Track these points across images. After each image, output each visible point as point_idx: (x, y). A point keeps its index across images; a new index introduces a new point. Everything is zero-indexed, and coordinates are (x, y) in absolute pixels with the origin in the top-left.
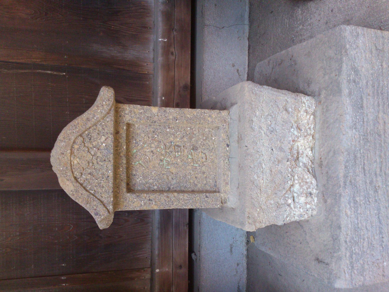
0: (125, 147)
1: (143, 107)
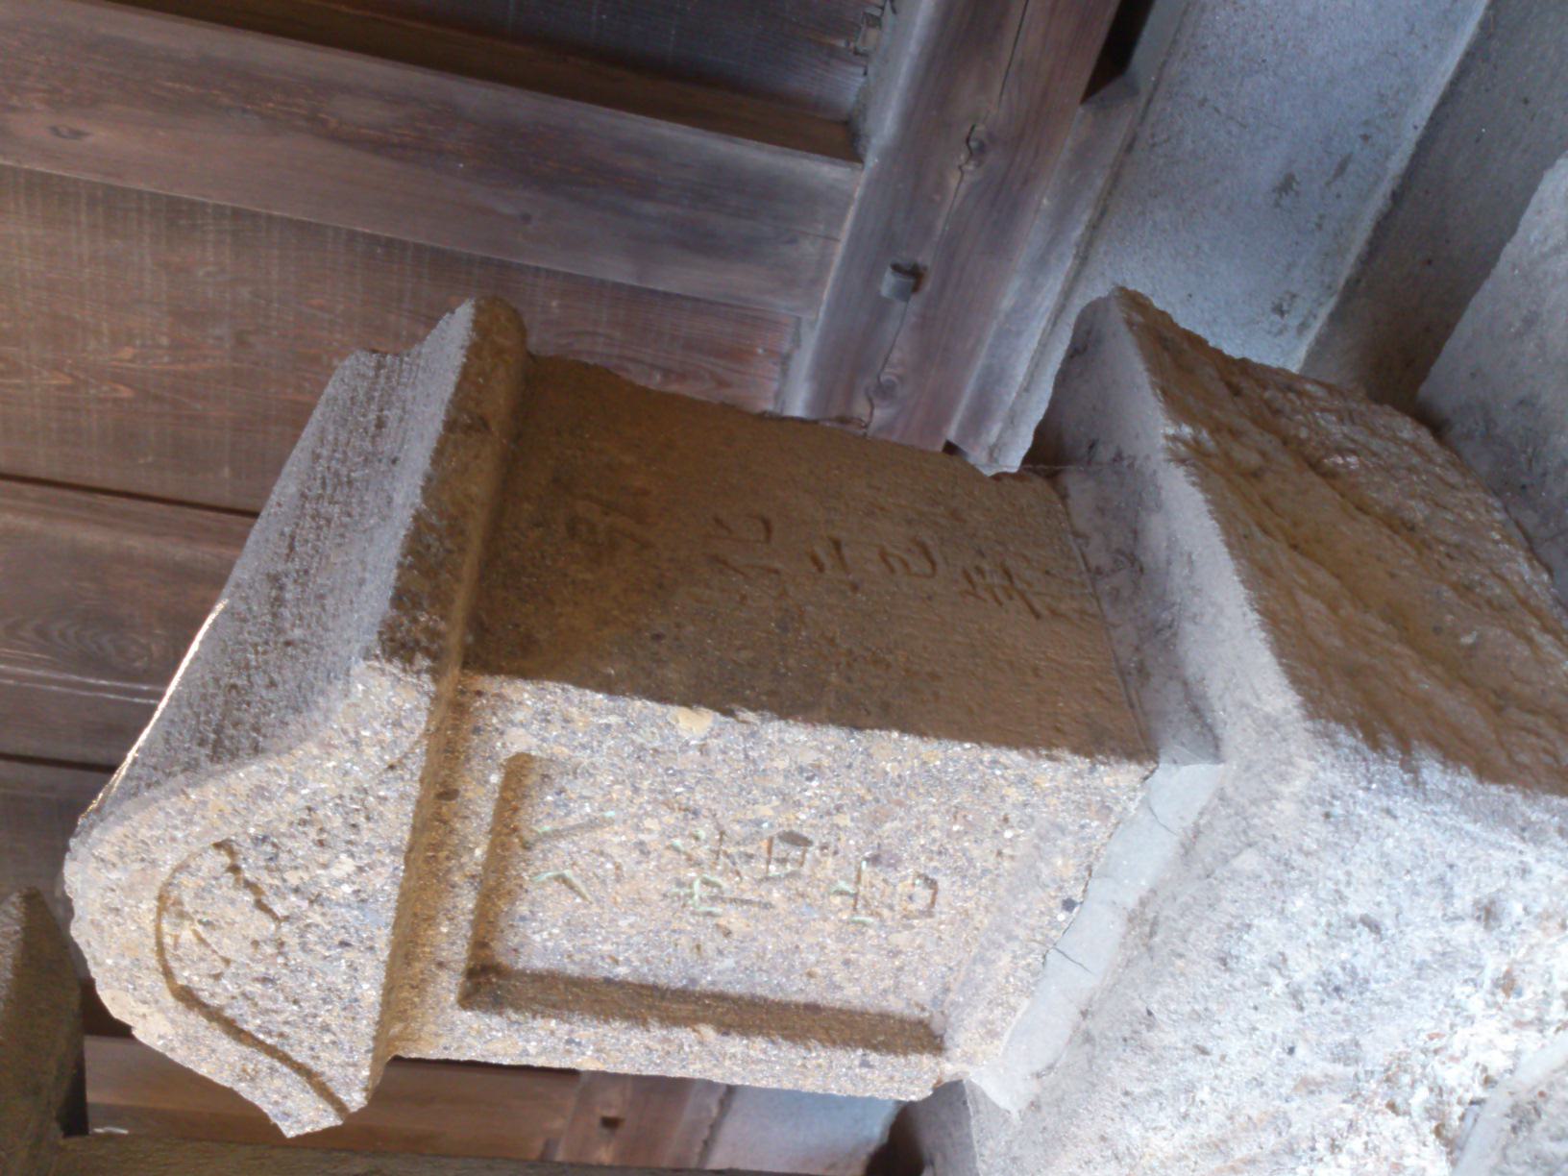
0: (478, 852)
1: (622, 702)
